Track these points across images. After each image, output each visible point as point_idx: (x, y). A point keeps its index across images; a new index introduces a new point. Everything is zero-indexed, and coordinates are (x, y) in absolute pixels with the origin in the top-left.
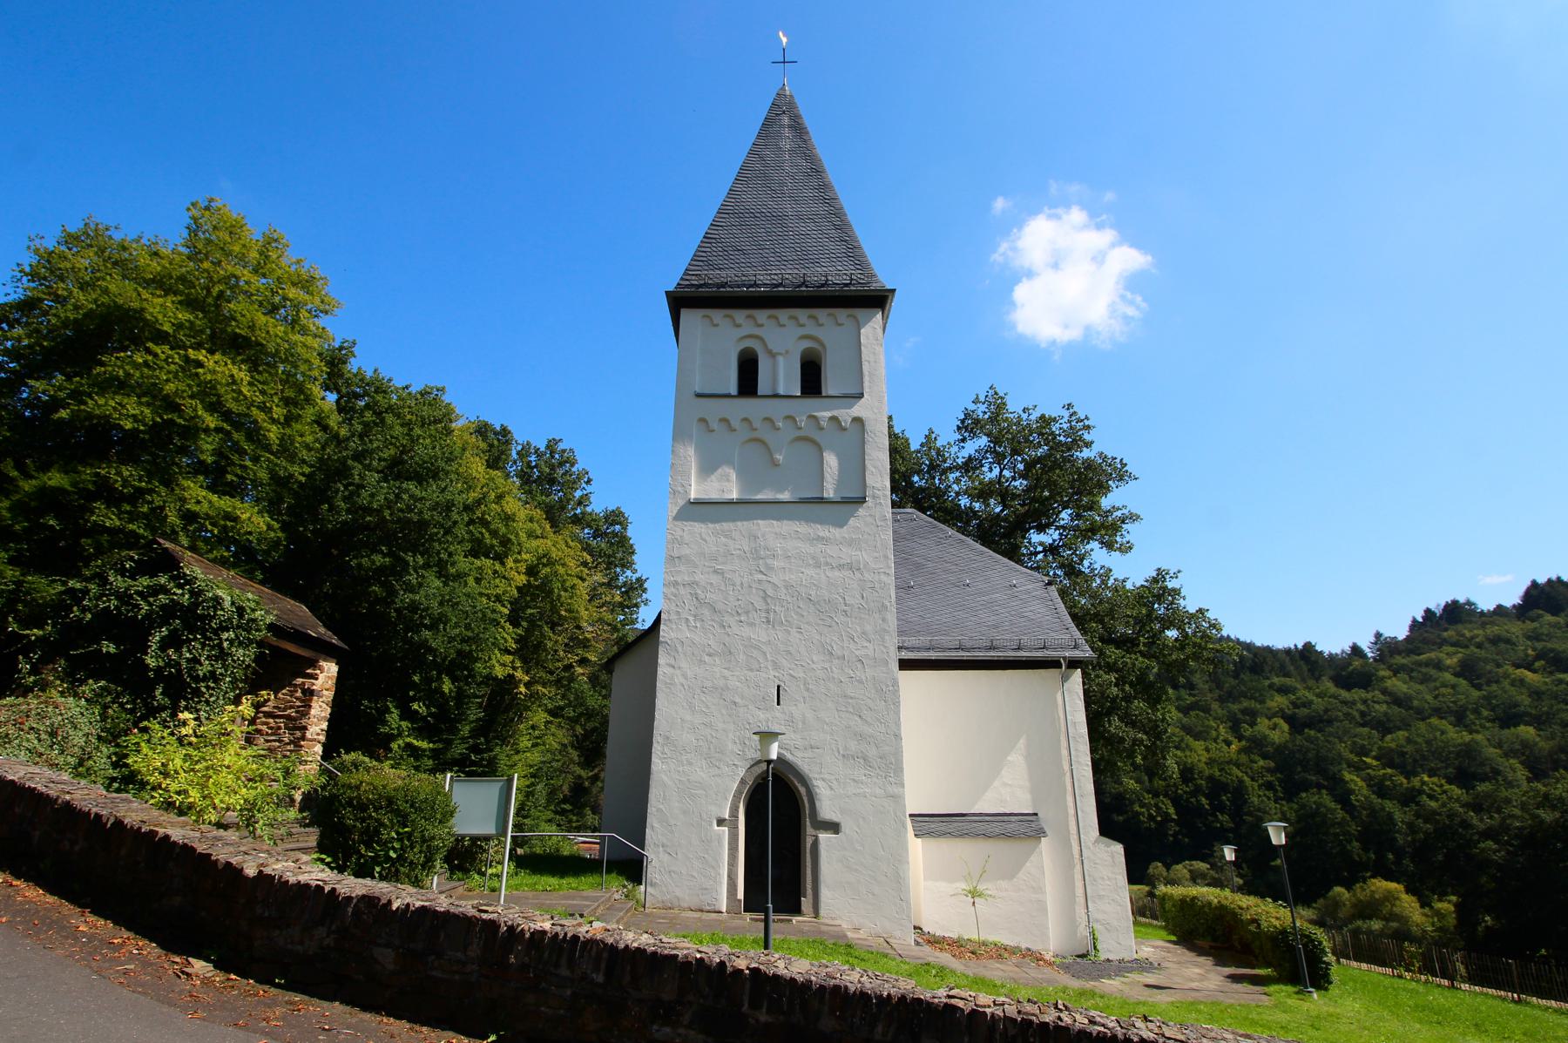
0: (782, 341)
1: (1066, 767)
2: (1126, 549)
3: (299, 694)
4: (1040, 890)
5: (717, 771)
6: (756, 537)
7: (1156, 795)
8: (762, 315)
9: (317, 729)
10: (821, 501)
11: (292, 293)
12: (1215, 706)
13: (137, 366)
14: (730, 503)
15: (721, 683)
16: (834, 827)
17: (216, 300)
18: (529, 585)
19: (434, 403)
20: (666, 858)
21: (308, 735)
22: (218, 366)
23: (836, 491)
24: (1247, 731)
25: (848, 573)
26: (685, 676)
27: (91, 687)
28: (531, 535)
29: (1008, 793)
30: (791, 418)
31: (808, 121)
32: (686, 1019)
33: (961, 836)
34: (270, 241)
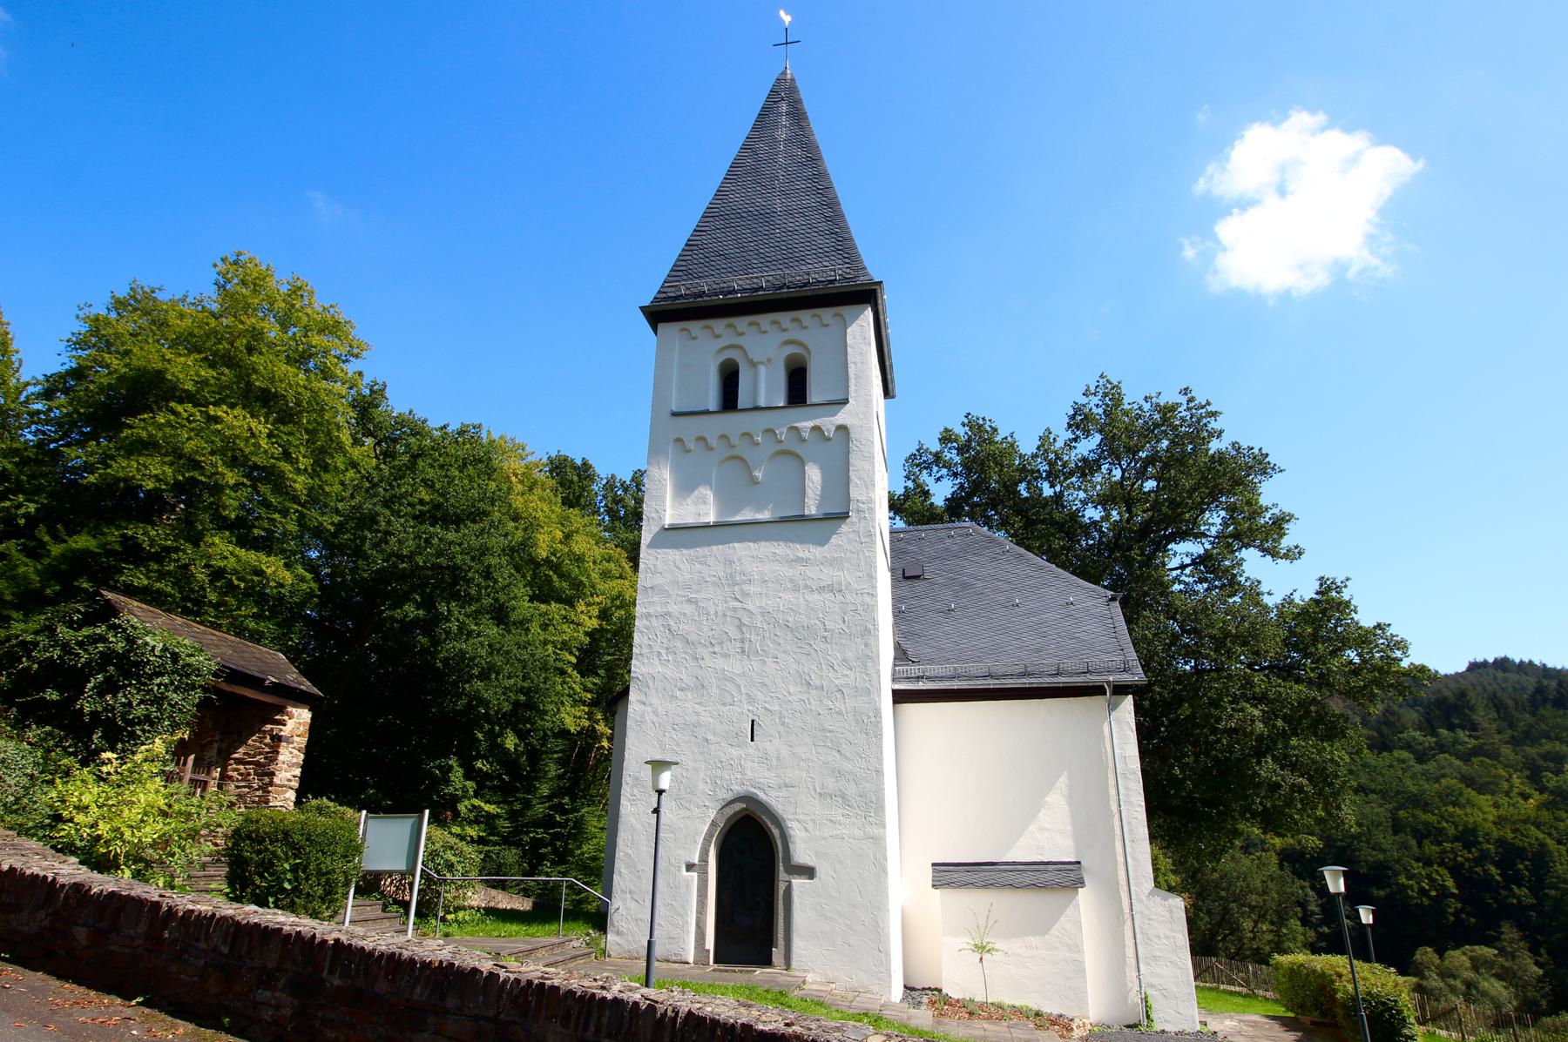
0: (764, 347)
1: (1114, 808)
2: (1294, 554)
3: (268, 740)
4: (1076, 947)
5: (687, 813)
6: (731, 562)
7: (1428, 863)
8: (741, 323)
9: (289, 775)
10: (803, 518)
11: (316, 339)
12: (1506, 750)
13: (160, 427)
14: (707, 526)
15: (693, 719)
16: (809, 872)
17: (246, 356)
18: (601, 630)
19: (475, 441)
20: (633, 905)
21: (276, 780)
22: (235, 420)
23: (818, 507)
24: (1551, 780)
25: (829, 596)
26: (655, 713)
27: (33, 733)
28: (606, 575)
29: (1047, 837)
30: (770, 431)
31: (809, 106)
32: (281, 984)
33: (984, 886)
34: (296, 290)
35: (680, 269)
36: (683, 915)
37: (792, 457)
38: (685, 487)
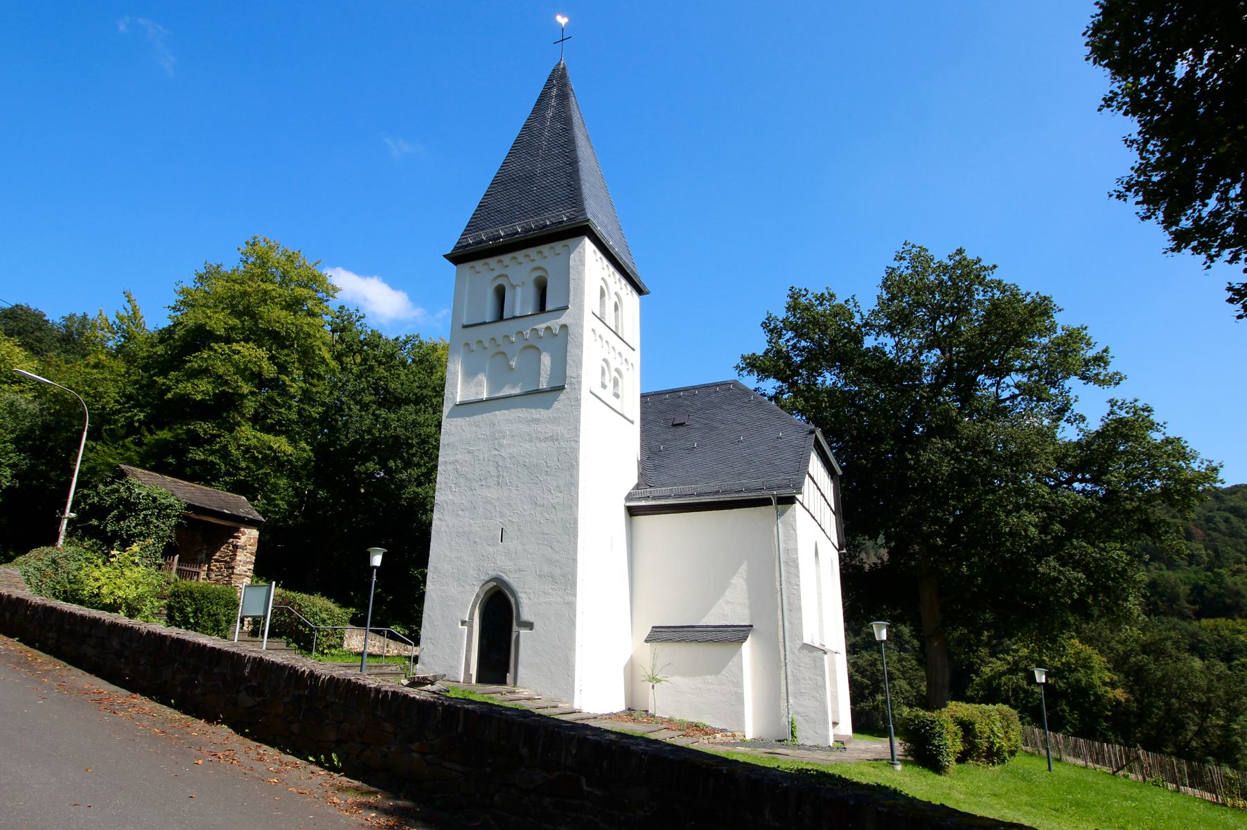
0: (519, 271)
4: (739, 684)
8: (506, 258)
14: (481, 401)
16: (530, 625)
22: (250, 352)
23: (548, 383)
25: (550, 443)
35: (472, 227)
36: (458, 653)
37: (533, 349)
38: (470, 373)
